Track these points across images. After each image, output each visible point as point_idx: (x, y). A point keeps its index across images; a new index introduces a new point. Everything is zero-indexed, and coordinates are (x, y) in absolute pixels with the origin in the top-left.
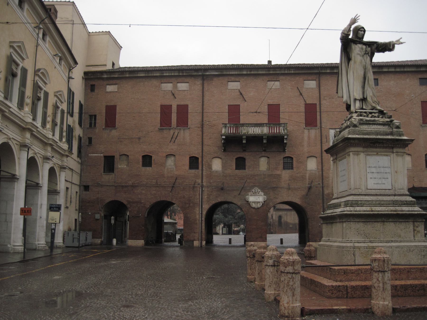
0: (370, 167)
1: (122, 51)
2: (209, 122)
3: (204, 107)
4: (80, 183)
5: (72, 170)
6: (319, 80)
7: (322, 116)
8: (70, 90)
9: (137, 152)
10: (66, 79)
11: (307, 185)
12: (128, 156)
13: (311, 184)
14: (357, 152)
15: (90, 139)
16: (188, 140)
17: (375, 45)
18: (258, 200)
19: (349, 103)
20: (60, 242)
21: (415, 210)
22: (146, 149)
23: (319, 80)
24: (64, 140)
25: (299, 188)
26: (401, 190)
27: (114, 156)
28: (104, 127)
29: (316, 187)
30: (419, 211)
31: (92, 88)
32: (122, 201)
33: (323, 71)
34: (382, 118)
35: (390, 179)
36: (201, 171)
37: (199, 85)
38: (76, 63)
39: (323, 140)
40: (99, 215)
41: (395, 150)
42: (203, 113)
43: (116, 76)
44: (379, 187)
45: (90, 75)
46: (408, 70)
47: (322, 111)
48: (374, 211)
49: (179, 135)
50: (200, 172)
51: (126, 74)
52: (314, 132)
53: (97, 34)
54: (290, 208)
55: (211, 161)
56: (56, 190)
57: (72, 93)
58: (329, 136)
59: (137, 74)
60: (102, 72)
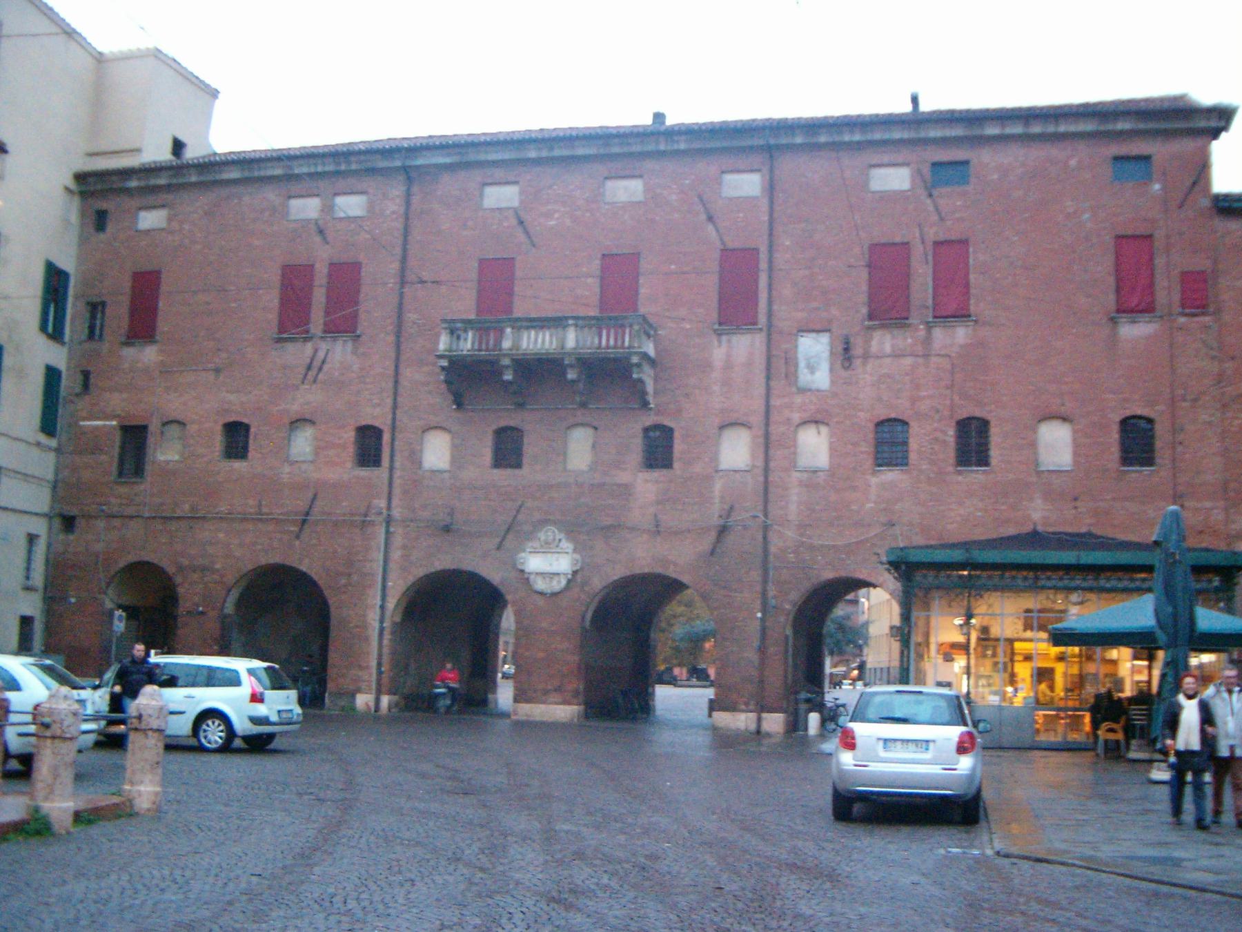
13: (728, 516)
18: (554, 569)
23: (771, 170)
25: (689, 531)
31: (100, 220)
33: (783, 141)
52: (744, 347)
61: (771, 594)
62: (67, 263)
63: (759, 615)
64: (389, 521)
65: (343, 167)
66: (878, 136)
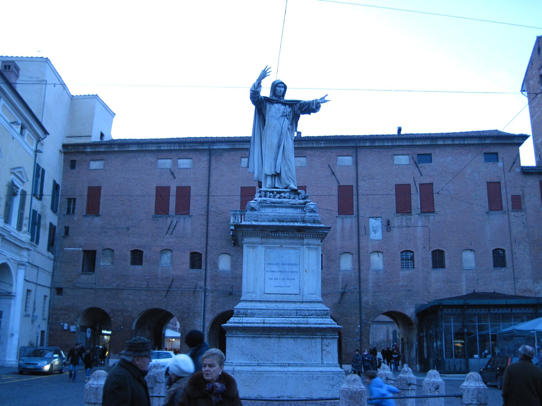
0: (269, 264)
1: (115, 119)
2: (216, 208)
3: (211, 189)
4: (52, 284)
5: (38, 267)
6: (356, 157)
7: (360, 201)
8: (38, 165)
9: (124, 246)
10: (32, 154)
11: (340, 290)
12: (113, 251)
13: (345, 288)
14: (253, 243)
15: (67, 229)
16: (189, 230)
17: (298, 105)
19: (260, 181)
20: (12, 359)
21: (325, 322)
22: (136, 242)
23: (356, 157)
24: (25, 229)
25: (330, 294)
26: (311, 296)
27: (96, 251)
28: (85, 214)
29: (352, 293)
30: (331, 324)
31: (73, 165)
32: (103, 309)
33: (361, 145)
34: (294, 198)
35: (297, 280)
36: (204, 271)
37: (206, 162)
38: (46, 133)
39: (360, 232)
40: (74, 327)
41: (305, 241)
42: (208, 196)
43: (103, 150)
44: (281, 290)
45: (70, 148)
46: (470, 142)
47: (359, 194)
48: (266, 323)
49: (177, 225)
50: (204, 273)
51: (114, 147)
52: (349, 222)
53: (82, 97)
54: (392, 320)
55: (218, 259)
56: (10, 293)
57: (41, 170)
58: (369, 227)
59: (128, 147)
60: (85, 145)
61: (363, 318)
62: (59, 182)
63: (359, 326)
64: (205, 291)
65: (182, 148)
66: (397, 144)
